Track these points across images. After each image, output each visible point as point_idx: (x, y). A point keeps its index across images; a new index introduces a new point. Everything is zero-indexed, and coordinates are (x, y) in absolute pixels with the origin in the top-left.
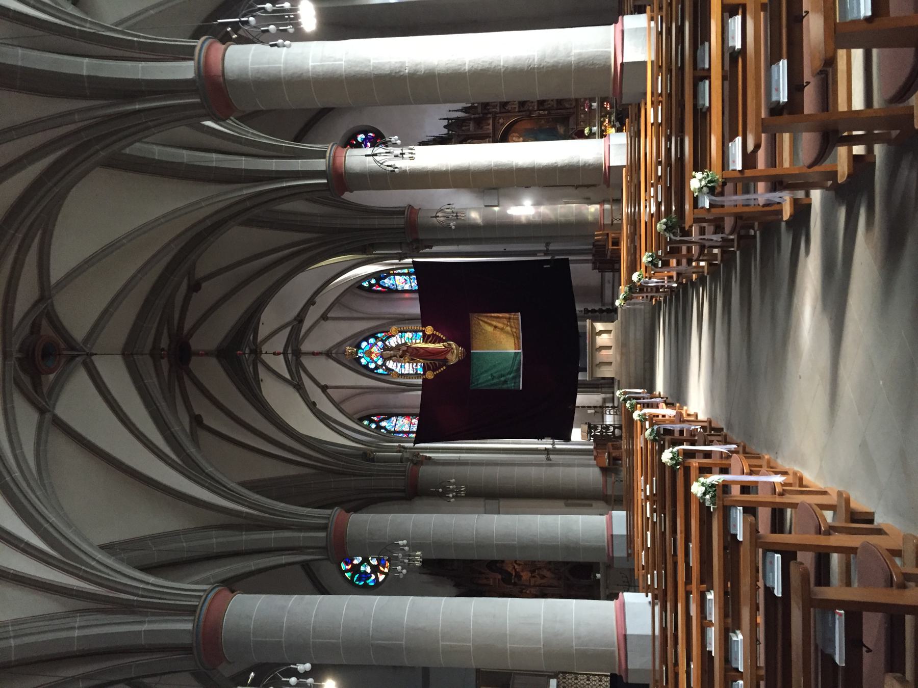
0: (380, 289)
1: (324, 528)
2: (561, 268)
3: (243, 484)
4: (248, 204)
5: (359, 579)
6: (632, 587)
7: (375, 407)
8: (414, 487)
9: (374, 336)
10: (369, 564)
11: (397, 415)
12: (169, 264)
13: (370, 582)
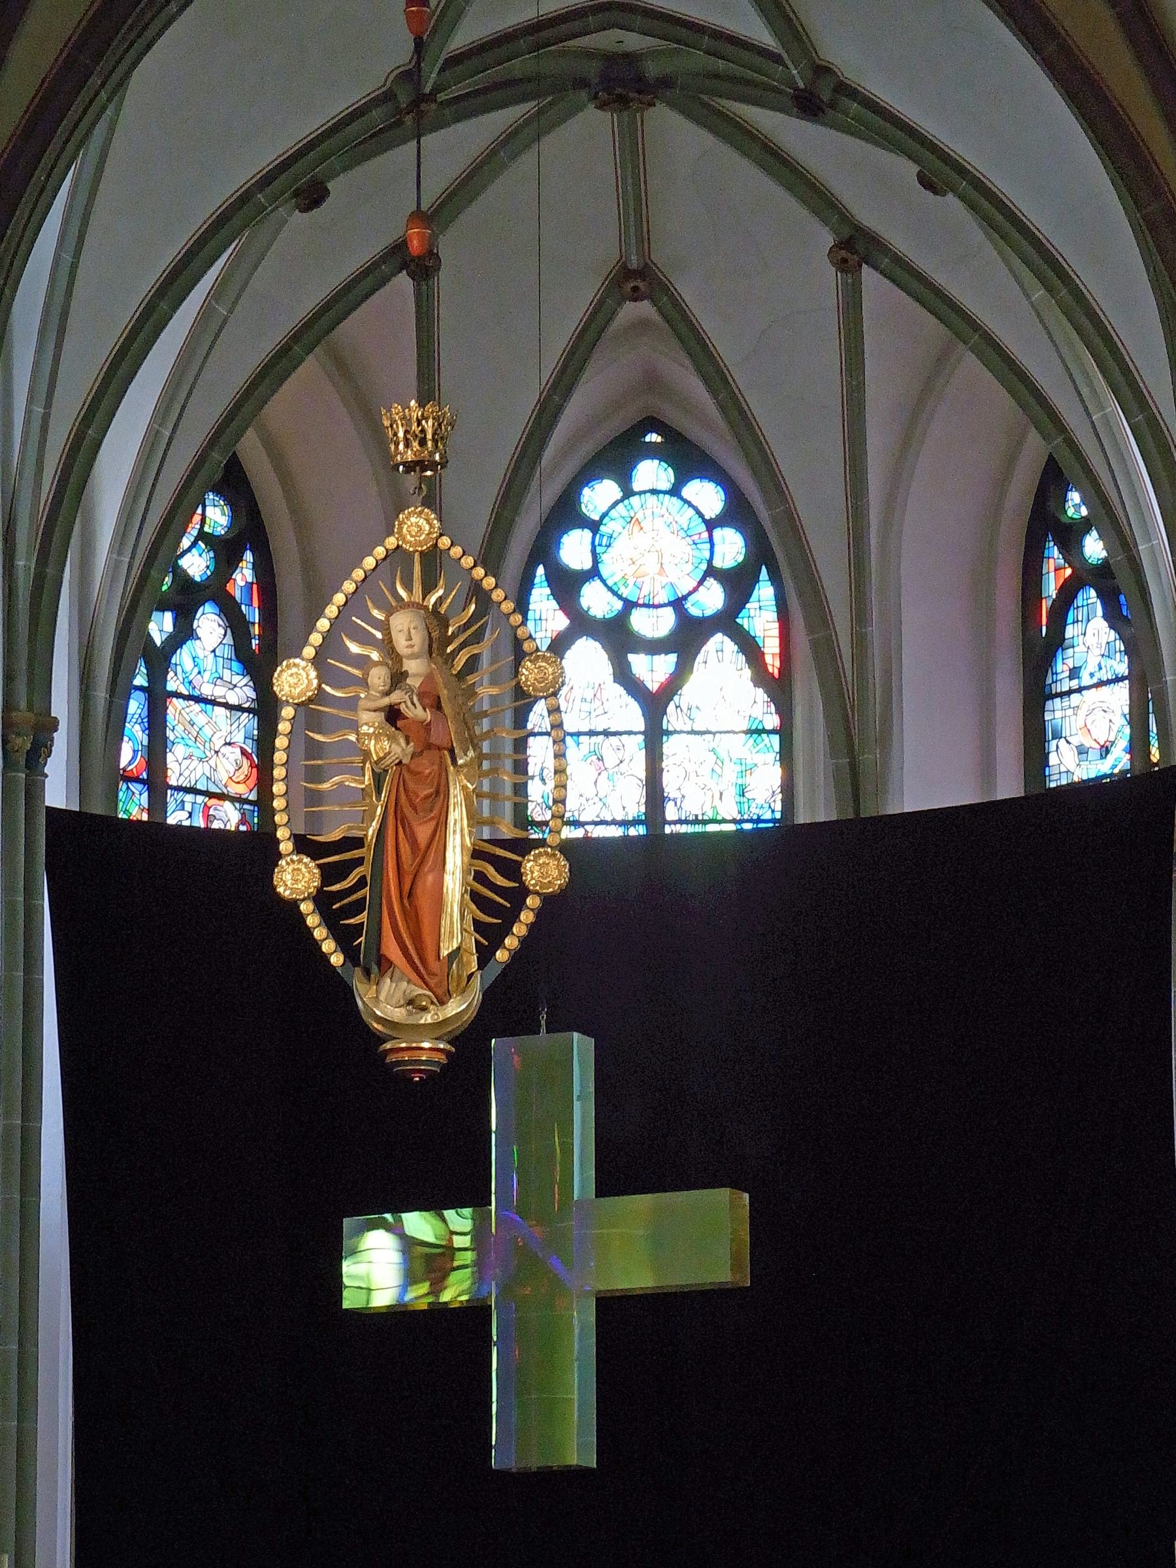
0: (1051, 588)
9: (760, 554)
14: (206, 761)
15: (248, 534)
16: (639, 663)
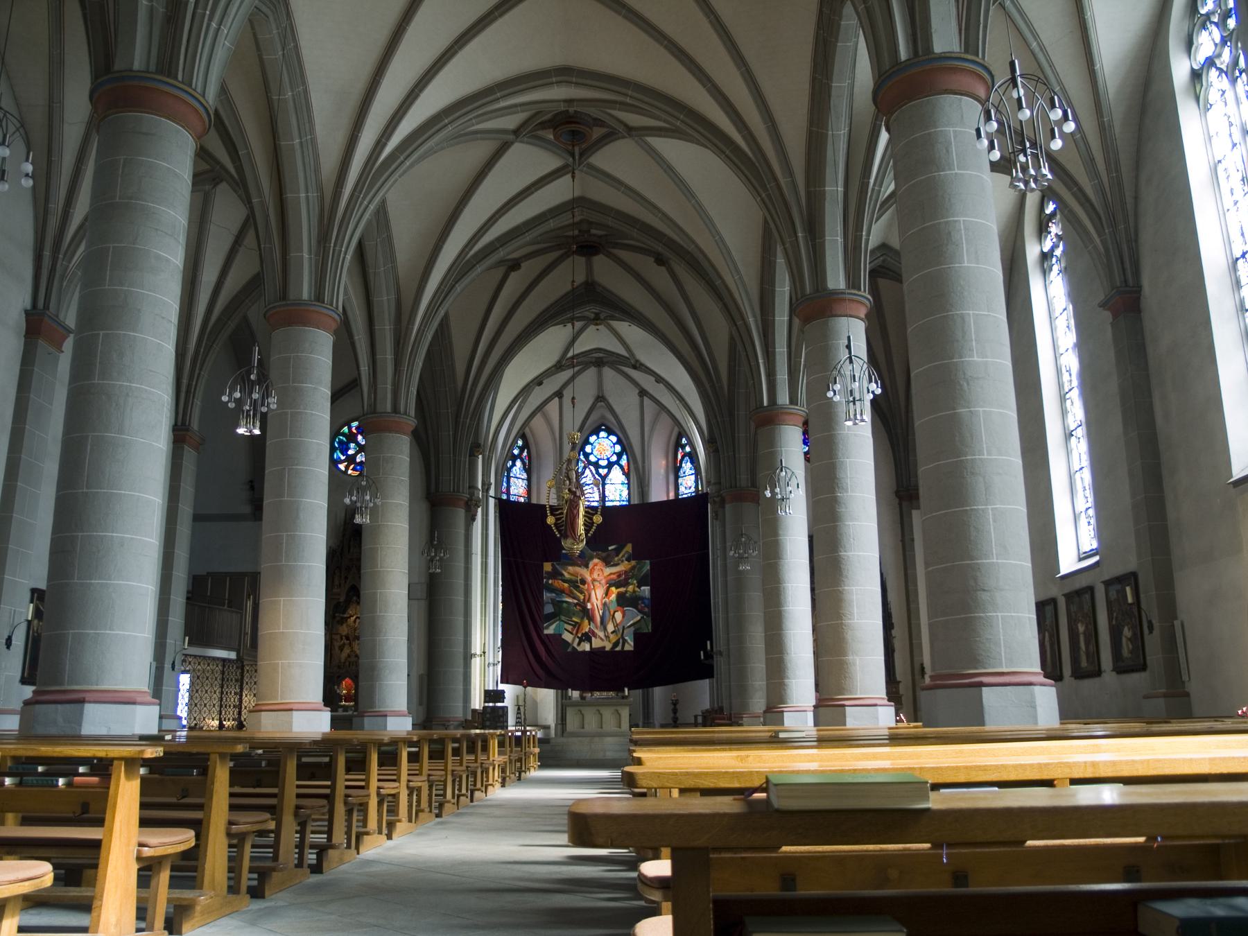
0: (679, 457)
1: (395, 410)
2: (706, 671)
3: (446, 316)
4: (739, 323)
5: (341, 442)
6: (335, 723)
7: (539, 456)
8: (441, 503)
9: (624, 450)
10: (357, 453)
11: (529, 479)
12: (674, 241)
13: (339, 455)
14: (518, 489)
15: (526, 446)
16: (601, 471)
